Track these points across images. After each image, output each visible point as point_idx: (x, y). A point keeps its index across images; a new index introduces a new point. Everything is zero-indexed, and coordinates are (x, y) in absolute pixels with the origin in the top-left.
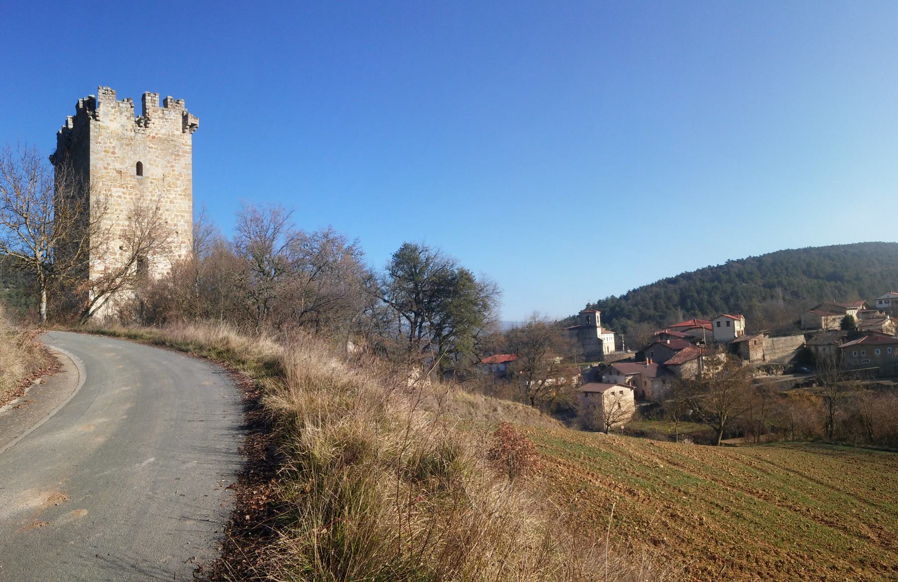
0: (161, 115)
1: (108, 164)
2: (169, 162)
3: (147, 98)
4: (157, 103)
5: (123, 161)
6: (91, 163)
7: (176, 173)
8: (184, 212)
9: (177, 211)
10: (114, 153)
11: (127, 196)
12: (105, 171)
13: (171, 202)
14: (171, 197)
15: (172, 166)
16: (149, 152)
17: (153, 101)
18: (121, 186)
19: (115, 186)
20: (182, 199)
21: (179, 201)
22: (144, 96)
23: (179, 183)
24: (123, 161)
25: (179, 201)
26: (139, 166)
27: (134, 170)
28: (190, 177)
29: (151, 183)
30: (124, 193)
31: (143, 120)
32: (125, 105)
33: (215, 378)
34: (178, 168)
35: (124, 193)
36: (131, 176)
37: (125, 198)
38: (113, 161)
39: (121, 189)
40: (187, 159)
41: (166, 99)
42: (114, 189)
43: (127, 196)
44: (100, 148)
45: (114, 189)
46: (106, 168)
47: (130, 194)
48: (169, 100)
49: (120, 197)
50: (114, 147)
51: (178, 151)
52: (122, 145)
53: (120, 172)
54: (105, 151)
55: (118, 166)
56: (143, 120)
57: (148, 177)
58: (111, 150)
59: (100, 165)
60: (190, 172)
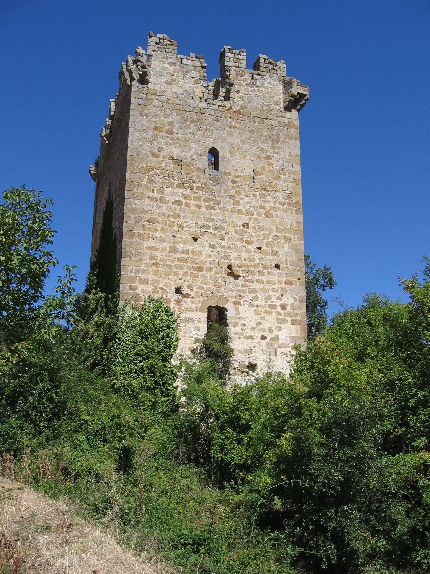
0: (249, 81)
1: (160, 149)
2: (262, 150)
3: (228, 54)
4: (243, 64)
5: (185, 145)
6: (130, 145)
7: (275, 167)
8: (290, 231)
9: (278, 230)
10: (170, 132)
11: (192, 202)
12: (152, 160)
13: (268, 215)
14: (267, 206)
15: (268, 158)
16: (231, 134)
17: (238, 61)
18: (181, 185)
19: (171, 185)
20: (285, 211)
21: (280, 213)
22: (222, 55)
23: (280, 184)
24: (185, 145)
25: (280, 213)
26: (214, 152)
27: (204, 162)
28: (299, 176)
29: (234, 182)
30: (186, 197)
31: (222, 84)
32: (192, 62)
33: (181, 334)
34: (277, 161)
35: (186, 197)
36: (199, 170)
37: (187, 205)
38: (167, 144)
39: (183, 191)
40: (294, 147)
41: (258, 60)
42: (168, 190)
43: (192, 202)
44: (146, 124)
45: (168, 190)
46: (155, 155)
47: (197, 199)
48: (262, 61)
49: (179, 203)
50: (171, 123)
51: (277, 134)
52: (184, 121)
53: (179, 162)
54: (156, 128)
55: (176, 152)
56: (222, 84)
57: (228, 173)
58: (167, 127)
59: (145, 149)
60: (298, 168)
